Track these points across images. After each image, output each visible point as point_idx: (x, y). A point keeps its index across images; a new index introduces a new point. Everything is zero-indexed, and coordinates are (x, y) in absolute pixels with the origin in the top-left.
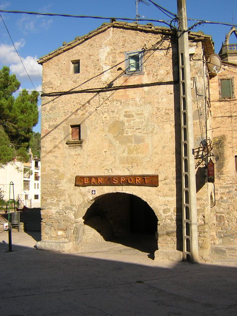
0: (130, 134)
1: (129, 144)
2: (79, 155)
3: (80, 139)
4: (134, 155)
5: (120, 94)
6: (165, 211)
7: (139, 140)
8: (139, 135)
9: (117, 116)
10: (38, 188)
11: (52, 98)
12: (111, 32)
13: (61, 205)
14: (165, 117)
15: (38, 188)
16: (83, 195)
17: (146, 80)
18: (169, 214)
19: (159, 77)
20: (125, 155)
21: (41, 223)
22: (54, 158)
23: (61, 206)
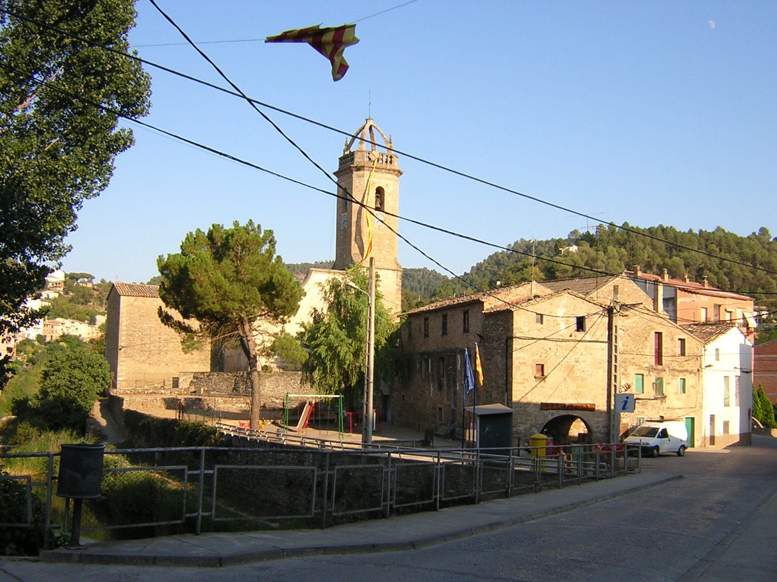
0: (578, 375)
1: (578, 382)
2: (543, 387)
3: (543, 375)
4: (580, 389)
5: (350, 342)
6: (597, 428)
7: (583, 380)
8: (584, 376)
9: (569, 360)
10: (712, 418)
11: (535, 341)
12: (566, 297)
13: (528, 424)
14: (599, 365)
15: (712, 418)
16: (546, 417)
17: (588, 337)
18: (599, 429)
19: (597, 337)
20: (574, 389)
21: (699, 446)
22: (523, 388)
23: (528, 425)
